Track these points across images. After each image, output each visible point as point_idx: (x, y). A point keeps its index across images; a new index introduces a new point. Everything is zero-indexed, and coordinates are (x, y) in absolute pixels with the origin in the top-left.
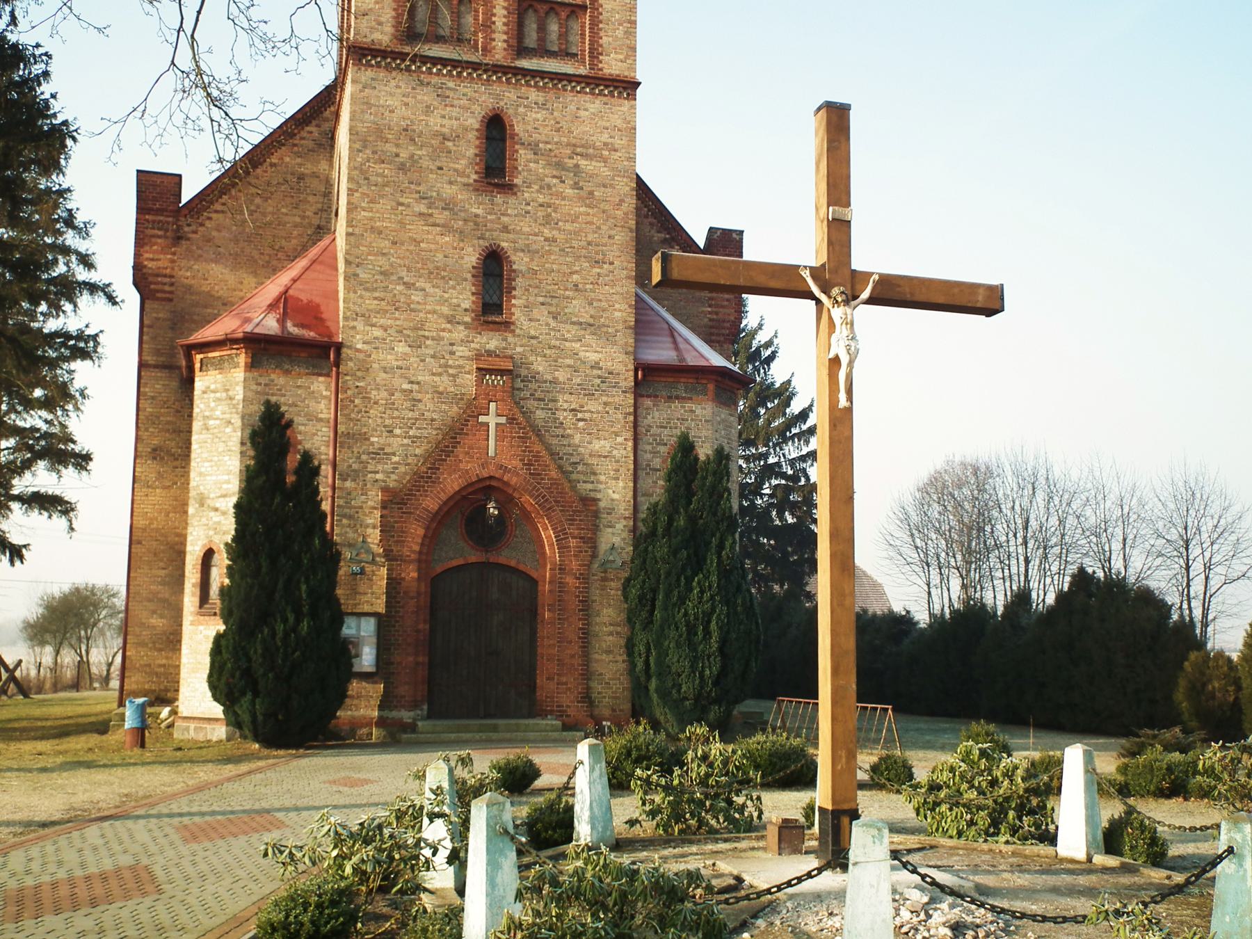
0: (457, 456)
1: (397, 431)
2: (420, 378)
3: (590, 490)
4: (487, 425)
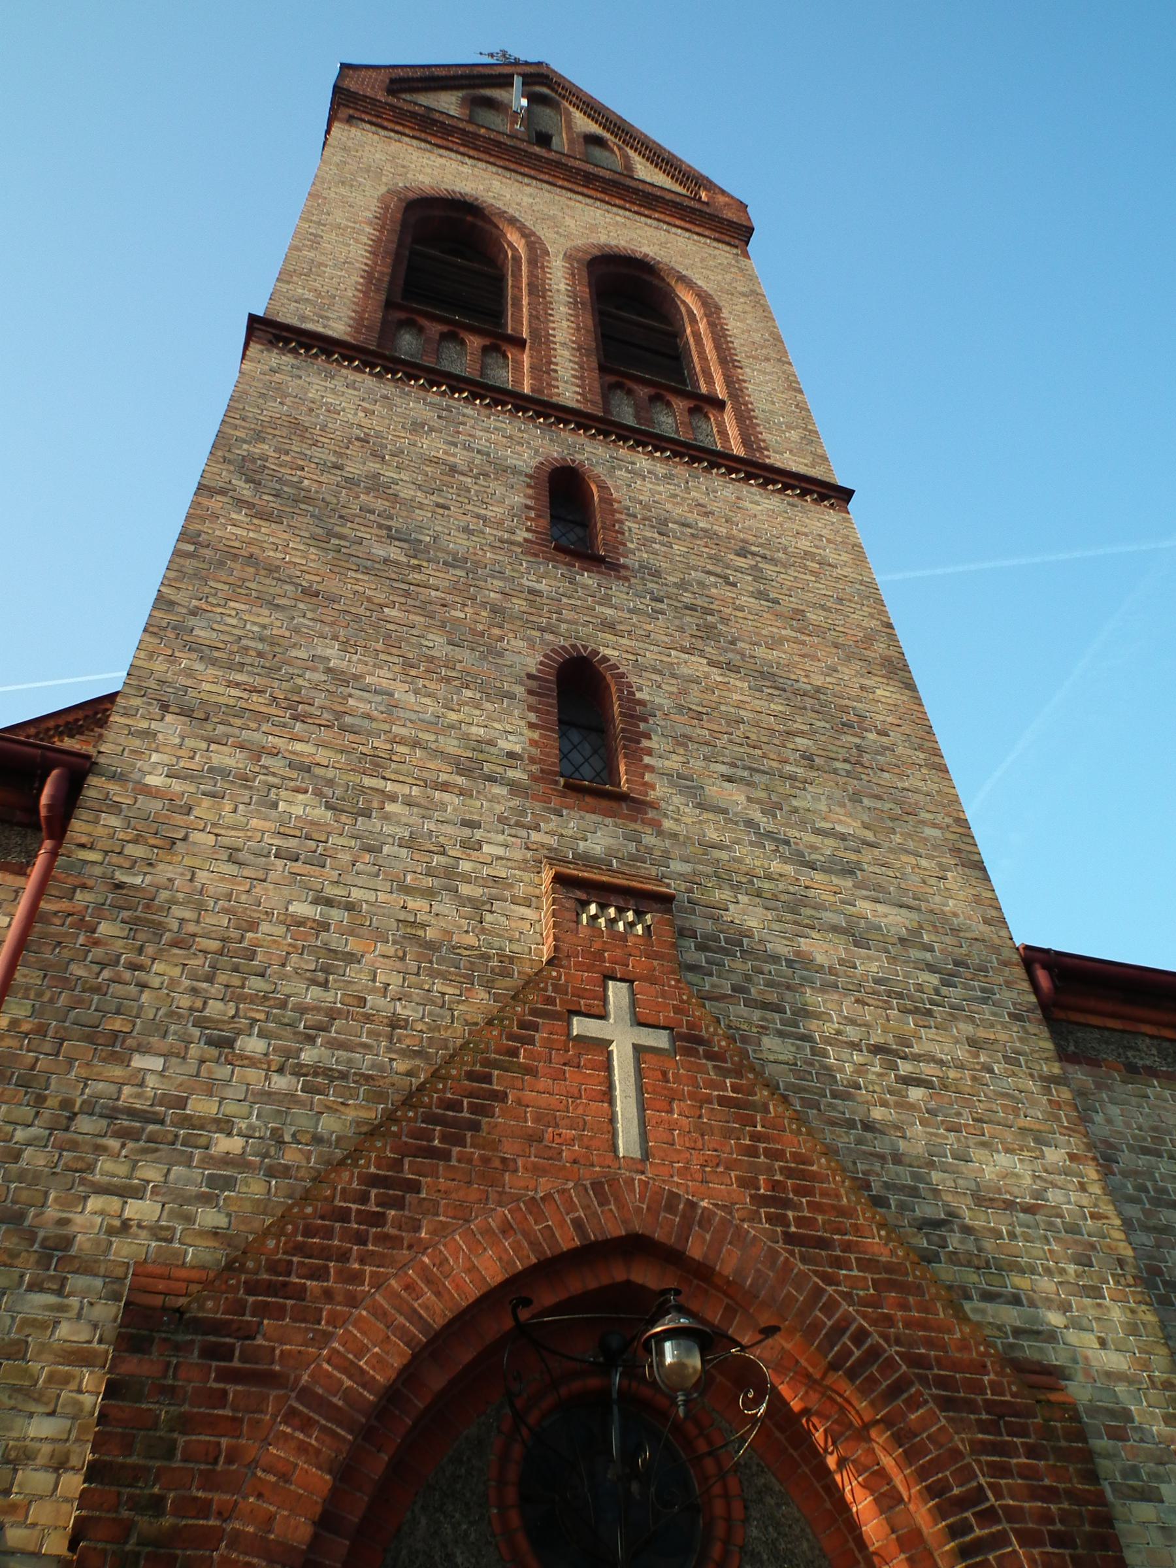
0: (494, 1145)
1: (253, 1045)
2: (356, 894)
3: (1017, 1332)
4: (603, 1045)
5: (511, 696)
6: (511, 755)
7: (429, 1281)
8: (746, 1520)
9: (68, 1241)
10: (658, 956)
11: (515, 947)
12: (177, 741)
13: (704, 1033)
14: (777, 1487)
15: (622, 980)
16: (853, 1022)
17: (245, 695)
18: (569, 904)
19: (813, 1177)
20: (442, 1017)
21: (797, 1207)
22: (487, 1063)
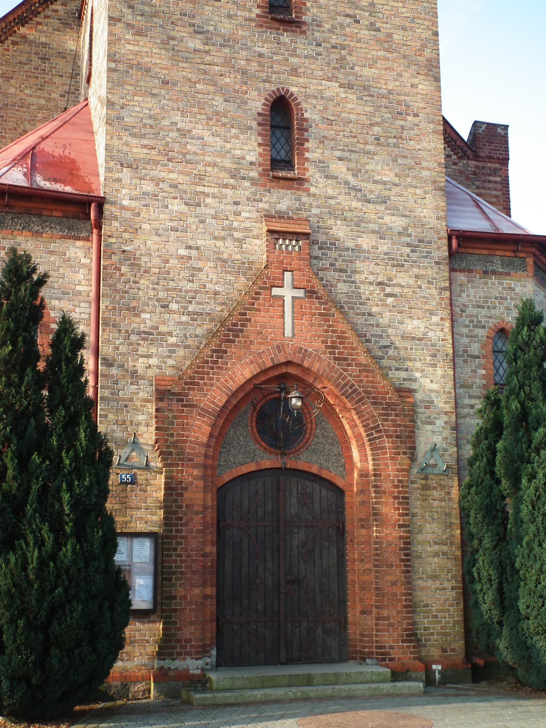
0: (247, 337)
3: (404, 380)
5: (250, 128)
6: (251, 163)
7: (231, 379)
8: (316, 429)
9: (136, 372)
10: (302, 259)
11: (254, 258)
12: (129, 181)
13: (316, 289)
14: (326, 420)
15: (290, 271)
16: (372, 273)
17: (148, 151)
18: (272, 241)
19: (346, 338)
20: (230, 289)
21: (339, 348)
22: (245, 309)
